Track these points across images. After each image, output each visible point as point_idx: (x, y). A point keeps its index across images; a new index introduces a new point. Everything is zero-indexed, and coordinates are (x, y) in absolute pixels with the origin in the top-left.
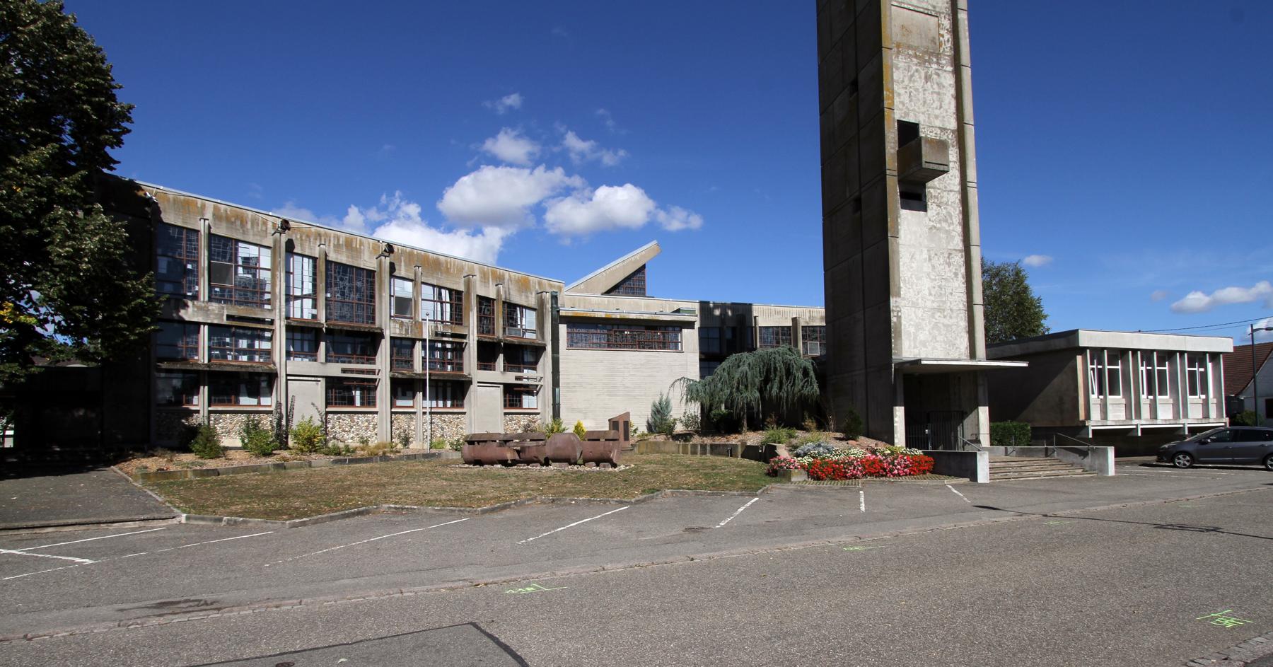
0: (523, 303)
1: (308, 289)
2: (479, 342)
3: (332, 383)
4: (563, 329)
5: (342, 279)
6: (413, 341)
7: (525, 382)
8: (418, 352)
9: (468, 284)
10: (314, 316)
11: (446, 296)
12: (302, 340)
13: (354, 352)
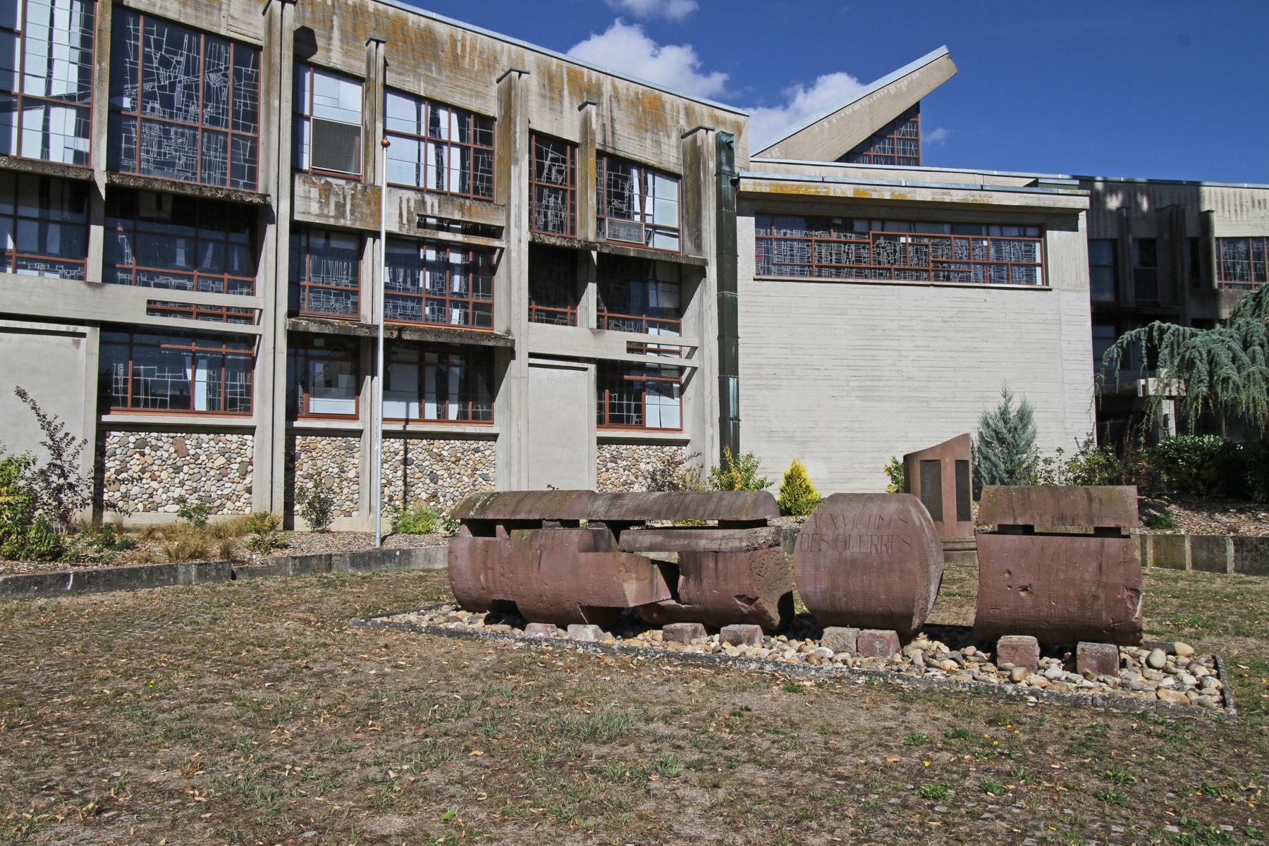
0: (648, 157)
1: (66, 80)
2: (532, 245)
3: (115, 334)
4: (746, 227)
5: (165, 63)
6: (360, 237)
7: (650, 359)
8: (375, 268)
9: (508, 99)
10: (80, 157)
11: (449, 125)
12: (44, 222)
13: (195, 260)
